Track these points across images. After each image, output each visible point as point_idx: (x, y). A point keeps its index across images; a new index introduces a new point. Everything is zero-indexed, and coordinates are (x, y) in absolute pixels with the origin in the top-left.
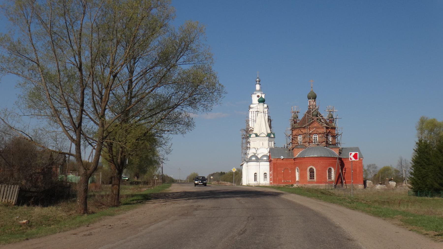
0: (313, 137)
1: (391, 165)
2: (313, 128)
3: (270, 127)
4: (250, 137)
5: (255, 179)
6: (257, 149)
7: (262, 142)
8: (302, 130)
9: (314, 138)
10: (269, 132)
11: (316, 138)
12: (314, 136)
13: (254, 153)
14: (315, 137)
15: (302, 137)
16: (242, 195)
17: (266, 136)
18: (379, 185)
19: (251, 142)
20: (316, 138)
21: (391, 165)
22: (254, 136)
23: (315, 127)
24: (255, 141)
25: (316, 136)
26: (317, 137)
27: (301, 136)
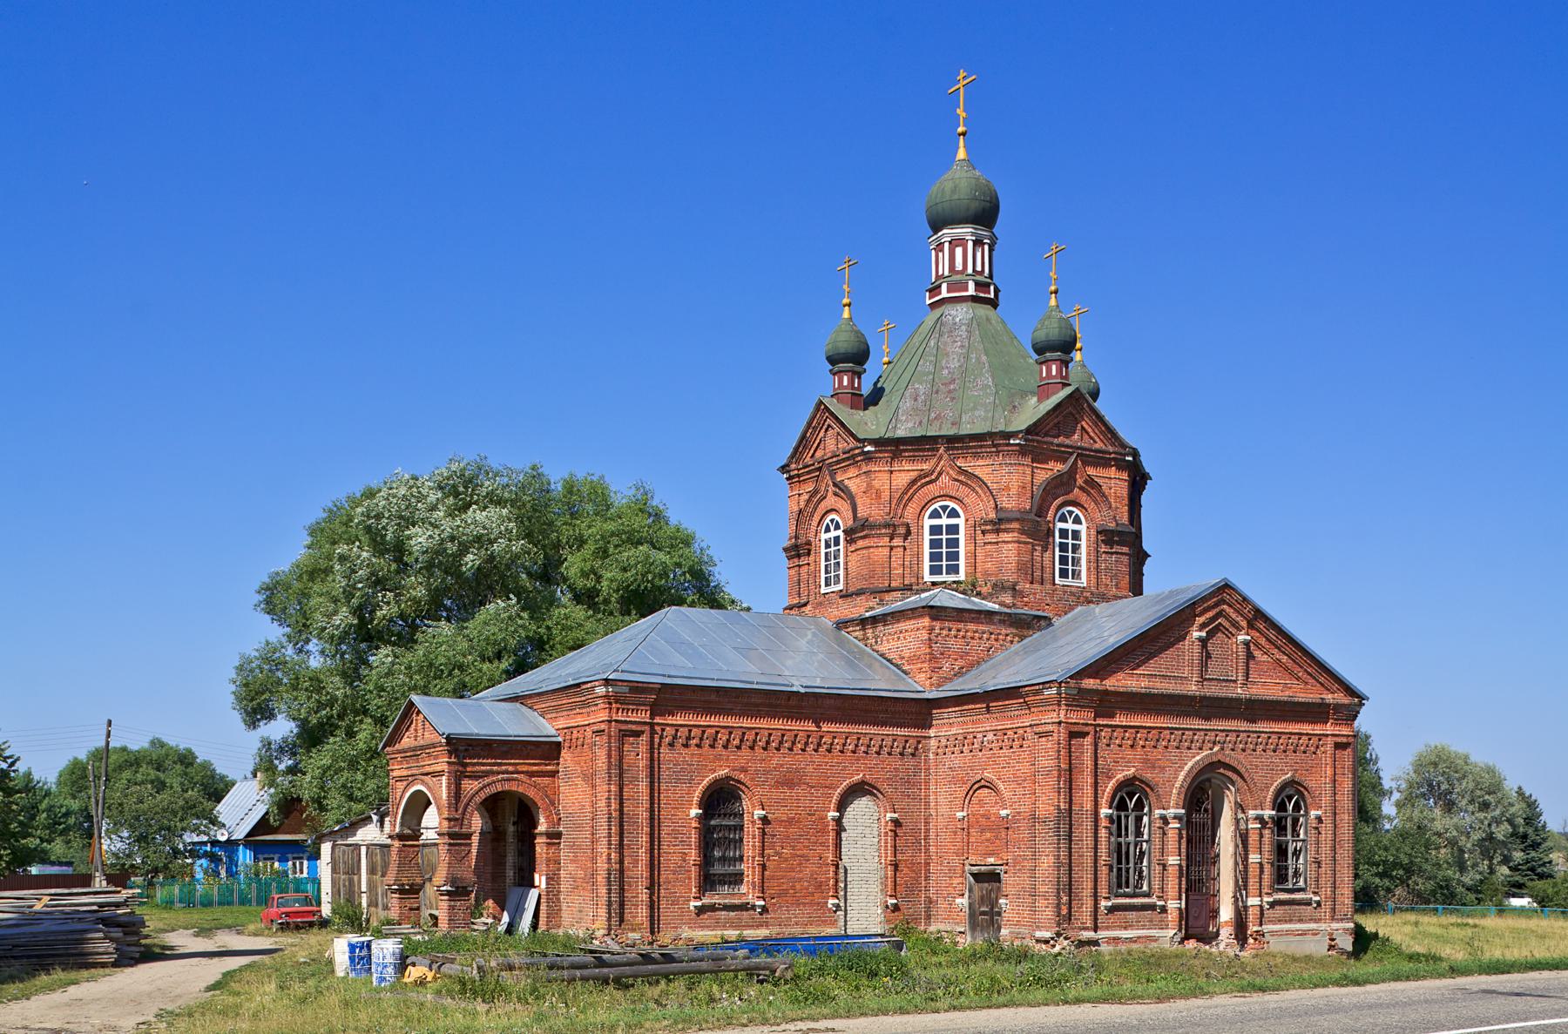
0: (928, 523)
11: (953, 529)
12: (935, 515)
14: (944, 521)
27: (954, 514)
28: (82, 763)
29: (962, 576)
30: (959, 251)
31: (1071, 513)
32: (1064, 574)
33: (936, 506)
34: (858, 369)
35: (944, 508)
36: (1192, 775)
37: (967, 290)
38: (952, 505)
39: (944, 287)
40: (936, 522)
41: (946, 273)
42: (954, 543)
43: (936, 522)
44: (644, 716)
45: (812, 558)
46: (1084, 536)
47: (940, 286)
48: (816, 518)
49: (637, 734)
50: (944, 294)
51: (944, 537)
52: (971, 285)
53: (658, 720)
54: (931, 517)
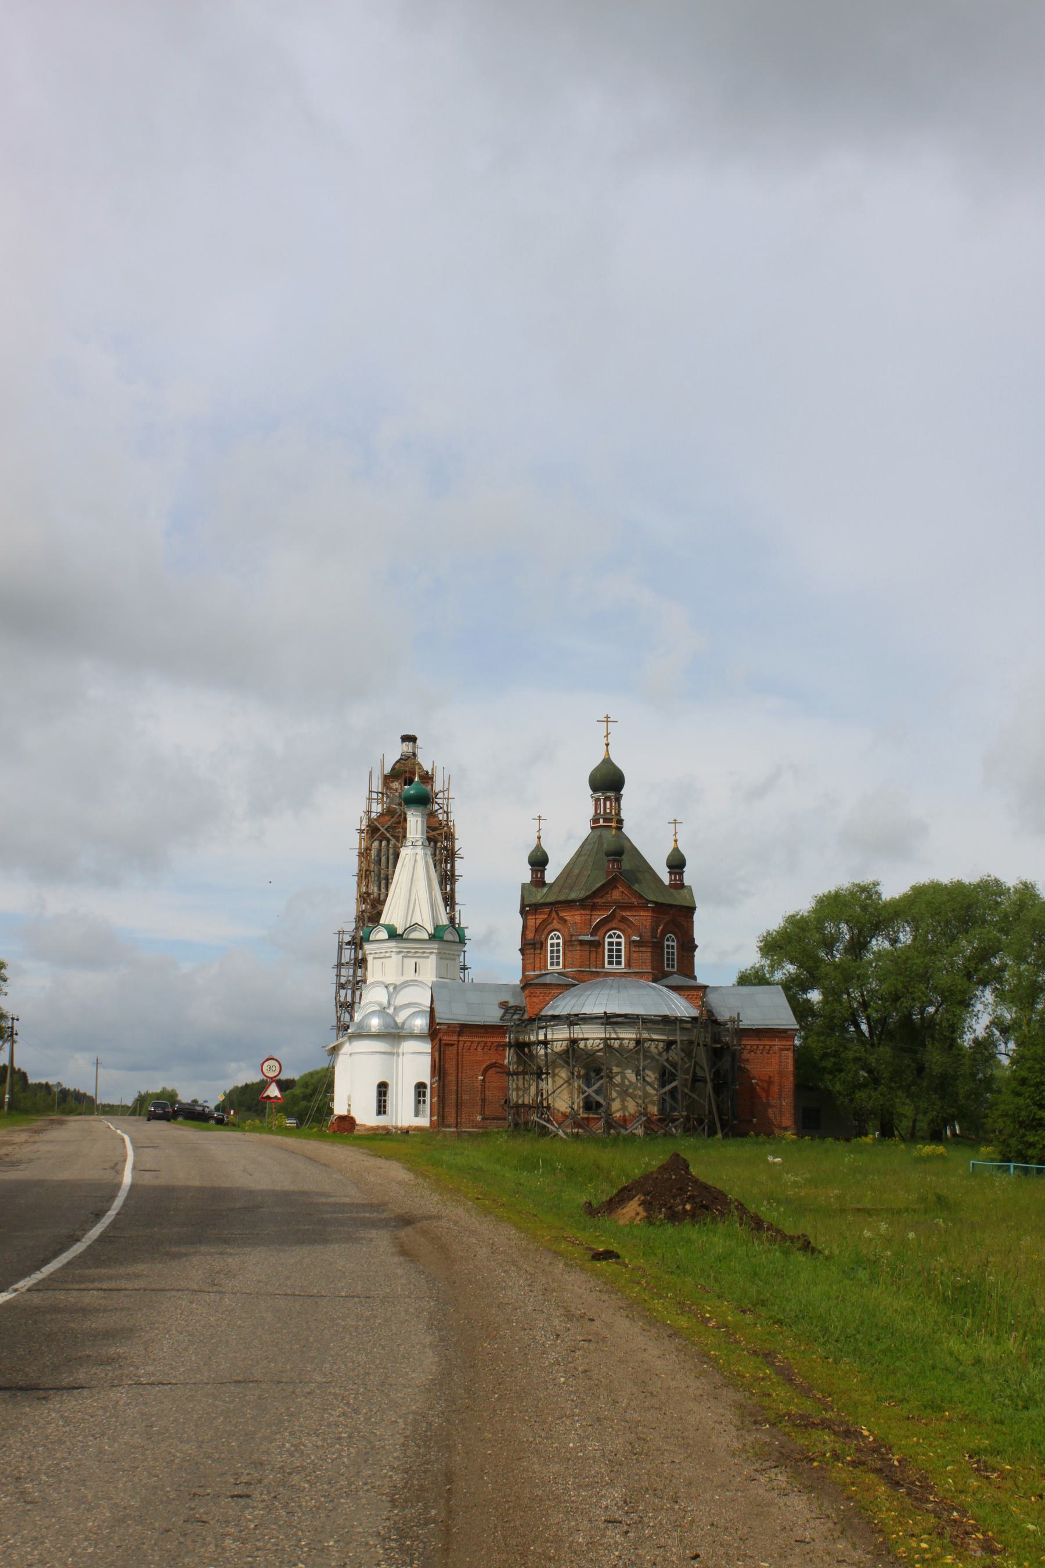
0: (607, 940)
1: (739, 1014)
2: (605, 907)
3: (449, 900)
4: (368, 940)
5: (381, 1109)
6: (391, 989)
7: (413, 961)
8: (562, 914)
9: (611, 944)
10: (444, 921)
11: (619, 944)
12: (610, 937)
13: (380, 1004)
14: (615, 940)
15: (561, 941)
16: (711, 1096)
17: (430, 939)
18: (691, 1169)
19: (370, 959)
20: (619, 944)
21: (739, 1014)
22: (384, 935)
23: (616, 902)
24: (387, 955)
25: (619, 937)
26: (622, 940)
27: (558, 938)
28: (812, 1004)
29: (666, 969)
30: (608, 803)
31: (555, 935)
32: (668, 966)
33: (611, 932)
34: (680, 871)
35: (615, 934)
36: (436, 1111)
37: (599, 823)
38: (618, 932)
39: (601, 820)
40: (552, 941)
41: (602, 813)
42: (619, 950)
43: (552, 941)
44: (455, 1038)
45: (542, 952)
46: (676, 954)
47: (599, 819)
48: (546, 932)
49: (452, 1045)
50: (601, 822)
51: (615, 947)
52: (601, 820)
53: (461, 1039)
54: (608, 938)
